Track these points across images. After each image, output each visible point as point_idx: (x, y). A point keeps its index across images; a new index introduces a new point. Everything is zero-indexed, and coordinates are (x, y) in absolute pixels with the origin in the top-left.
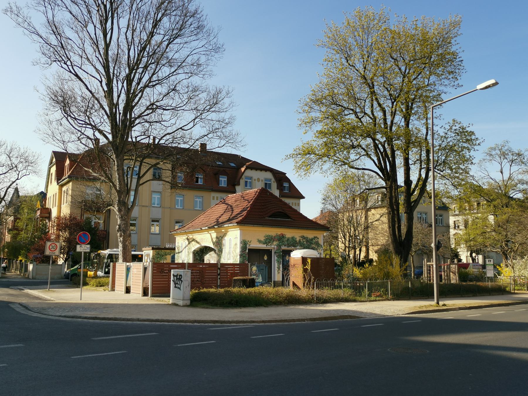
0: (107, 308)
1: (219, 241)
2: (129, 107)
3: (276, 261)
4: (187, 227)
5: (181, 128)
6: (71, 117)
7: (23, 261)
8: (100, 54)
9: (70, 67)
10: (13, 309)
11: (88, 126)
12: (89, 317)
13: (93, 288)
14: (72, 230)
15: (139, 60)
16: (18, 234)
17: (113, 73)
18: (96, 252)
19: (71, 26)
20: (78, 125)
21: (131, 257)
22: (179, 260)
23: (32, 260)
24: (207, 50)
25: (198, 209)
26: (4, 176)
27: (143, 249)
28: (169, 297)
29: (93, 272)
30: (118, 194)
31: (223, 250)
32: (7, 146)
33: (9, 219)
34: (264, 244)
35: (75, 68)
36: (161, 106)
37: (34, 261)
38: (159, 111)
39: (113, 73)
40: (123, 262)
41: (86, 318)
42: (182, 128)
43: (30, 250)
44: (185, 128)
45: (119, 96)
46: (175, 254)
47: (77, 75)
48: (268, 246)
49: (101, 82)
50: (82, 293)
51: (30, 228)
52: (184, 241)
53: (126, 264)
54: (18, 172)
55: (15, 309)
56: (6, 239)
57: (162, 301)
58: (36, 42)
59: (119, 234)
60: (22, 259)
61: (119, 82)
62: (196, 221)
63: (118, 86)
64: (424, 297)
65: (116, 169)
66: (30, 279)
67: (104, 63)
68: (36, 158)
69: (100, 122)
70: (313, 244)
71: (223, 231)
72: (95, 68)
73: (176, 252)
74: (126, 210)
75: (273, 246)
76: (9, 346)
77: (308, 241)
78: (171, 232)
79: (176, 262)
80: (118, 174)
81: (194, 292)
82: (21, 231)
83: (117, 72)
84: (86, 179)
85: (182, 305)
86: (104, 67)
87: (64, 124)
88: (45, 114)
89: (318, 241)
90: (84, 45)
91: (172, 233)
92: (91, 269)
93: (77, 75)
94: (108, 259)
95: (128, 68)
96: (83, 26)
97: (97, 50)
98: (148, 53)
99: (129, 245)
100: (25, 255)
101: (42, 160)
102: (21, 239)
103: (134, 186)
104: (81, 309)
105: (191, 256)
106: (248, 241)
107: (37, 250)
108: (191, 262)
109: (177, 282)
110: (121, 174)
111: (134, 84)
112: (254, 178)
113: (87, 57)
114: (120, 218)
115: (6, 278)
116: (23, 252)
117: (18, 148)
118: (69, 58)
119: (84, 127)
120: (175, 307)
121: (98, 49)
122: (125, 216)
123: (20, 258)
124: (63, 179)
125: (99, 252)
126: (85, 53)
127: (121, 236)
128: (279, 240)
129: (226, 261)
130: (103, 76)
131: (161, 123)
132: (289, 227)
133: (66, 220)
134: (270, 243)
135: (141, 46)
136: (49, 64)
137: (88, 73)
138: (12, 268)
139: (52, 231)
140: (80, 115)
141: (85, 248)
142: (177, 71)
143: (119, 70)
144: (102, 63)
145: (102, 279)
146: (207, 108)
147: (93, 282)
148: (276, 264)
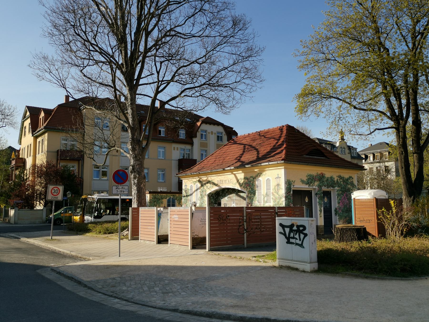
1: (250, 182)
3: (318, 204)
25: (161, 158)
29: (79, 217)
31: (257, 192)
34: (307, 184)
52: (195, 184)
53: (157, 209)
59: (132, 175)
66: (12, 224)
68: (11, 111)
70: (349, 184)
71: (256, 170)
74: (141, 149)
77: (344, 181)
80: (131, 109)
89: (353, 181)
99: (144, 187)
101: (18, 113)
105: (206, 199)
106: (292, 181)
107: (18, 196)
112: (208, 131)
114: (133, 158)
122: (139, 156)
124: (37, 131)
127: (135, 178)
128: (320, 180)
129: (262, 204)
134: (311, 183)
148: (318, 207)
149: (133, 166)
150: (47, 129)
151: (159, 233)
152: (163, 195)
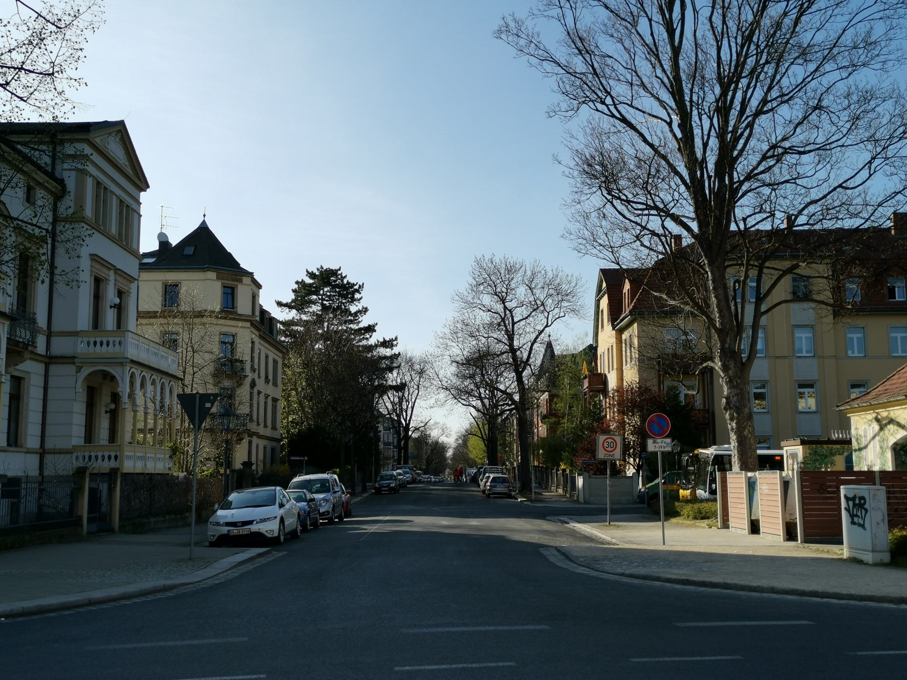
0: (712, 562)
2: (726, 161)
4: (873, 394)
5: (840, 186)
6: (622, 200)
7: (568, 472)
8: (664, 70)
9: (612, 108)
10: (545, 558)
11: (653, 212)
12: (675, 579)
13: (688, 522)
14: (645, 411)
15: (740, 65)
16: (558, 423)
17: (691, 101)
18: (691, 452)
19: (610, 31)
20: (634, 213)
21: (757, 462)
22: (861, 465)
23: (581, 470)
24: (887, 7)
26: (524, 323)
27: (783, 444)
28: (840, 542)
30: (718, 337)
32: (526, 270)
33: (542, 397)
35: (620, 107)
36: (793, 146)
37: (585, 471)
38: (790, 159)
39: (691, 101)
40: (741, 470)
41: (668, 580)
42: (844, 185)
43: (576, 452)
44: (850, 184)
45: (705, 145)
46: (852, 453)
47: (624, 120)
49: (670, 124)
50: (665, 532)
51: (577, 411)
52: (870, 425)
53: (746, 475)
54: (546, 314)
55: (548, 557)
56: (539, 433)
57: (828, 552)
58: (550, 75)
59: (727, 415)
60: (565, 467)
61: (704, 117)
62: (895, 380)
63: (702, 125)
65: (711, 288)
66: (581, 503)
67: (672, 86)
68: (574, 284)
69: (673, 200)
72: (658, 99)
73: (853, 448)
76: (526, 627)
78: (838, 406)
79: (855, 469)
80: (715, 297)
81: (899, 534)
82: (563, 417)
83: (698, 97)
84: (657, 313)
85: (871, 562)
86: (672, 94)
87: (610, 215)
88: (575, 202)
90: (634, 60)
91: (841, 408)
92: (683, 484)
93: (624, 120)
94: (713, 465)
95: (718, 85)
96: (629, 25)
97: (658, 65)
98: (758, 46)
99: (749, 436)
100: (569, 461)
102: (564, 432)
103: (748, 320)
104: (662, 563)
105: (889, 455)
108: (891, 470)
109: (855, 513)
110: (722, 297)
111: (734, 114)
113: (642, 83)
114: (727, 383)
115: (543, 501)
116: (565, 454)
117: (543, 272)
118: (609, 90)
119: (646, 215)
120: (856, 566)
121: (660, 61)
122: (736, 379)
123: (563, 467)
124: (621, 318)
125: (696, 452)
126: (638, 76)
127: (732, 419)
130: (672, 109)
131: (795, 183)
133: (632, 393)
135: (743, 35)
136: (575, 109)
137: (644, 112)
138: (552, 484)
139: (611, 415)
140: (637, 194)
141: (663, 444)
142: (821, 69)
143: (701, 94)
144: (668, 86)
145: (704, 505)
146: (898, 133)
147: (687, 509)
149: (727, 398)
150: (637, 314)
151: (752, 515)
152: (834, 446)
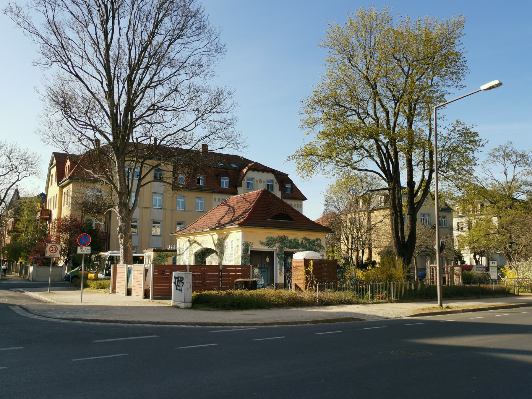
0: (108, 310)
1: (221, 243)
2: (130, 108)
3: (278, 263)
4: (188, 228)
5: (182, 129)
6: (72, 118)
7: (24, 263)
8: (101, 54)
9: (71, 68)
10: (13, 312)
11: (88, 127)
12: (90, 320)
13: (94, 290)
14: (73, 232)
15: (140, 61)
16: (18, 236)
17: (114, 74)
18: (97, 254)
19: (72, 26)
20: (78, 126)
21: (132, 259)
22: (180, 262)
23: (32, 262)
24: (208, 50)
25: (199, 210)
26: (4, 178)
27: (144, 251)
28: (171, 299)
29: (94, 274)
30: (118, 196)
31: (225, 252)
32: (7, 147)
33: (9, 221)
34: (266, 245)
35: (75, 68)
36: (163, 107)
37: (35, 263)
38: (161, 112)
39: (114, 74)
40: (124, 264)
41: (86, 320)
42: (184, 129)
43: (30, 252)
44: (187, 129)
45: (120, 97)
46: (176, 256)
47: (77, 76)
48: (270, 248)
49: (102, 83)
50: (83, 295)
51: (31, 230)
52: (186, 243)
53: (127, 266)
54: (18, 174)
55: (15, 311)
56: (6, 241)
57: (164, 303)
58: (36, 42)
59: (120, 235)
60: (22, 261)
61: (120, 83)
62: (198, 223)
63: (119, 87)
64: (427, 300)
65: (117, 171)
66: (30, 281)
67: (105, 64)
68: (36, 159)
69: (101, 123)
70: (315, 246)
71: (225, 232)
72: (96, 68)
73: (177, 254)
74: (127, 212)
75: (275, 248)
76: (10, 349)
77: (310, 243)
78: (172, 234)
79: (177, 264)
80: (118, 175)
81: (196, 294)
82: (22, 233)
83: (118, 72)
84: (86, 180)
85: (183, 307)
86: (105, 67)
87: (64, 125)
88: (45, 115)
89: (320, 243)
90: (84, 45)
91: (173, 235)
92: (91, 271)
93: (77, 76)
94: (108, 261)
95: (129, 69)
96: (83, 26)
97: (98, 50)
98: (149, 54)
99: (130, 247)
100: (25, 257)
101: (43, 161)
102: (22, 241)
103: (135, 188)
104: (82, 312)
105: (193, 258)
106: (250, 243)
107: (37, 252)
108: (193, 264)
109: (178, 284)
110: (122, 176)
111: (135, 84)
112: (256, 179)
113: (88, 58)
114: (121, 220)
115: (6, 280)
116: (23, 254)
117: (18, 150)
118: (70, 58)
119: (85, 128)
120: (176, 309)
121: (99, 49)
122: (126, 218)
123: (20, 260)
124: (63, 180)
125: (100, 254)
126: (86, 54)
127: (122, 238)
128: (281, 242)
129: (228, 263)
130: (104, 76)
131: (162, 124)
132: (292, 229)
133: (66, 221)
134: (272, 245)
135: (142, 46)
136: (50, 64)
137: (88, 74)
138: (12, 270)
139: (53, 233)
140: (81, 116)
141: (86, 250)
142: (178, 72)
143: (120, 71)
144: (103, 63)
145: (103, 281)
146: (209, 109)
147: (94, 284)
148: (278, 266)
